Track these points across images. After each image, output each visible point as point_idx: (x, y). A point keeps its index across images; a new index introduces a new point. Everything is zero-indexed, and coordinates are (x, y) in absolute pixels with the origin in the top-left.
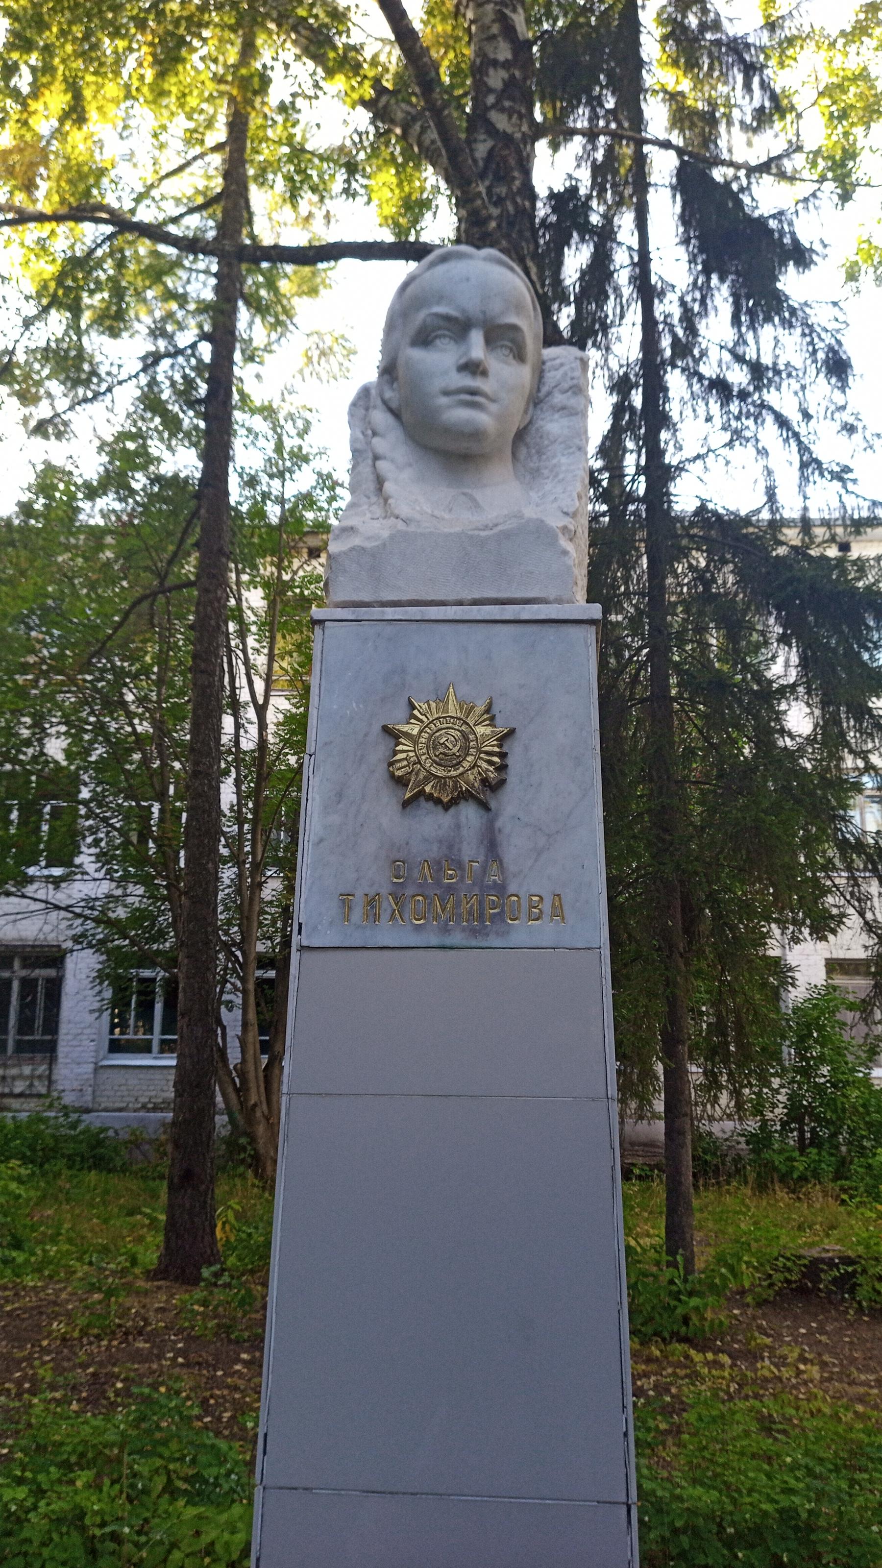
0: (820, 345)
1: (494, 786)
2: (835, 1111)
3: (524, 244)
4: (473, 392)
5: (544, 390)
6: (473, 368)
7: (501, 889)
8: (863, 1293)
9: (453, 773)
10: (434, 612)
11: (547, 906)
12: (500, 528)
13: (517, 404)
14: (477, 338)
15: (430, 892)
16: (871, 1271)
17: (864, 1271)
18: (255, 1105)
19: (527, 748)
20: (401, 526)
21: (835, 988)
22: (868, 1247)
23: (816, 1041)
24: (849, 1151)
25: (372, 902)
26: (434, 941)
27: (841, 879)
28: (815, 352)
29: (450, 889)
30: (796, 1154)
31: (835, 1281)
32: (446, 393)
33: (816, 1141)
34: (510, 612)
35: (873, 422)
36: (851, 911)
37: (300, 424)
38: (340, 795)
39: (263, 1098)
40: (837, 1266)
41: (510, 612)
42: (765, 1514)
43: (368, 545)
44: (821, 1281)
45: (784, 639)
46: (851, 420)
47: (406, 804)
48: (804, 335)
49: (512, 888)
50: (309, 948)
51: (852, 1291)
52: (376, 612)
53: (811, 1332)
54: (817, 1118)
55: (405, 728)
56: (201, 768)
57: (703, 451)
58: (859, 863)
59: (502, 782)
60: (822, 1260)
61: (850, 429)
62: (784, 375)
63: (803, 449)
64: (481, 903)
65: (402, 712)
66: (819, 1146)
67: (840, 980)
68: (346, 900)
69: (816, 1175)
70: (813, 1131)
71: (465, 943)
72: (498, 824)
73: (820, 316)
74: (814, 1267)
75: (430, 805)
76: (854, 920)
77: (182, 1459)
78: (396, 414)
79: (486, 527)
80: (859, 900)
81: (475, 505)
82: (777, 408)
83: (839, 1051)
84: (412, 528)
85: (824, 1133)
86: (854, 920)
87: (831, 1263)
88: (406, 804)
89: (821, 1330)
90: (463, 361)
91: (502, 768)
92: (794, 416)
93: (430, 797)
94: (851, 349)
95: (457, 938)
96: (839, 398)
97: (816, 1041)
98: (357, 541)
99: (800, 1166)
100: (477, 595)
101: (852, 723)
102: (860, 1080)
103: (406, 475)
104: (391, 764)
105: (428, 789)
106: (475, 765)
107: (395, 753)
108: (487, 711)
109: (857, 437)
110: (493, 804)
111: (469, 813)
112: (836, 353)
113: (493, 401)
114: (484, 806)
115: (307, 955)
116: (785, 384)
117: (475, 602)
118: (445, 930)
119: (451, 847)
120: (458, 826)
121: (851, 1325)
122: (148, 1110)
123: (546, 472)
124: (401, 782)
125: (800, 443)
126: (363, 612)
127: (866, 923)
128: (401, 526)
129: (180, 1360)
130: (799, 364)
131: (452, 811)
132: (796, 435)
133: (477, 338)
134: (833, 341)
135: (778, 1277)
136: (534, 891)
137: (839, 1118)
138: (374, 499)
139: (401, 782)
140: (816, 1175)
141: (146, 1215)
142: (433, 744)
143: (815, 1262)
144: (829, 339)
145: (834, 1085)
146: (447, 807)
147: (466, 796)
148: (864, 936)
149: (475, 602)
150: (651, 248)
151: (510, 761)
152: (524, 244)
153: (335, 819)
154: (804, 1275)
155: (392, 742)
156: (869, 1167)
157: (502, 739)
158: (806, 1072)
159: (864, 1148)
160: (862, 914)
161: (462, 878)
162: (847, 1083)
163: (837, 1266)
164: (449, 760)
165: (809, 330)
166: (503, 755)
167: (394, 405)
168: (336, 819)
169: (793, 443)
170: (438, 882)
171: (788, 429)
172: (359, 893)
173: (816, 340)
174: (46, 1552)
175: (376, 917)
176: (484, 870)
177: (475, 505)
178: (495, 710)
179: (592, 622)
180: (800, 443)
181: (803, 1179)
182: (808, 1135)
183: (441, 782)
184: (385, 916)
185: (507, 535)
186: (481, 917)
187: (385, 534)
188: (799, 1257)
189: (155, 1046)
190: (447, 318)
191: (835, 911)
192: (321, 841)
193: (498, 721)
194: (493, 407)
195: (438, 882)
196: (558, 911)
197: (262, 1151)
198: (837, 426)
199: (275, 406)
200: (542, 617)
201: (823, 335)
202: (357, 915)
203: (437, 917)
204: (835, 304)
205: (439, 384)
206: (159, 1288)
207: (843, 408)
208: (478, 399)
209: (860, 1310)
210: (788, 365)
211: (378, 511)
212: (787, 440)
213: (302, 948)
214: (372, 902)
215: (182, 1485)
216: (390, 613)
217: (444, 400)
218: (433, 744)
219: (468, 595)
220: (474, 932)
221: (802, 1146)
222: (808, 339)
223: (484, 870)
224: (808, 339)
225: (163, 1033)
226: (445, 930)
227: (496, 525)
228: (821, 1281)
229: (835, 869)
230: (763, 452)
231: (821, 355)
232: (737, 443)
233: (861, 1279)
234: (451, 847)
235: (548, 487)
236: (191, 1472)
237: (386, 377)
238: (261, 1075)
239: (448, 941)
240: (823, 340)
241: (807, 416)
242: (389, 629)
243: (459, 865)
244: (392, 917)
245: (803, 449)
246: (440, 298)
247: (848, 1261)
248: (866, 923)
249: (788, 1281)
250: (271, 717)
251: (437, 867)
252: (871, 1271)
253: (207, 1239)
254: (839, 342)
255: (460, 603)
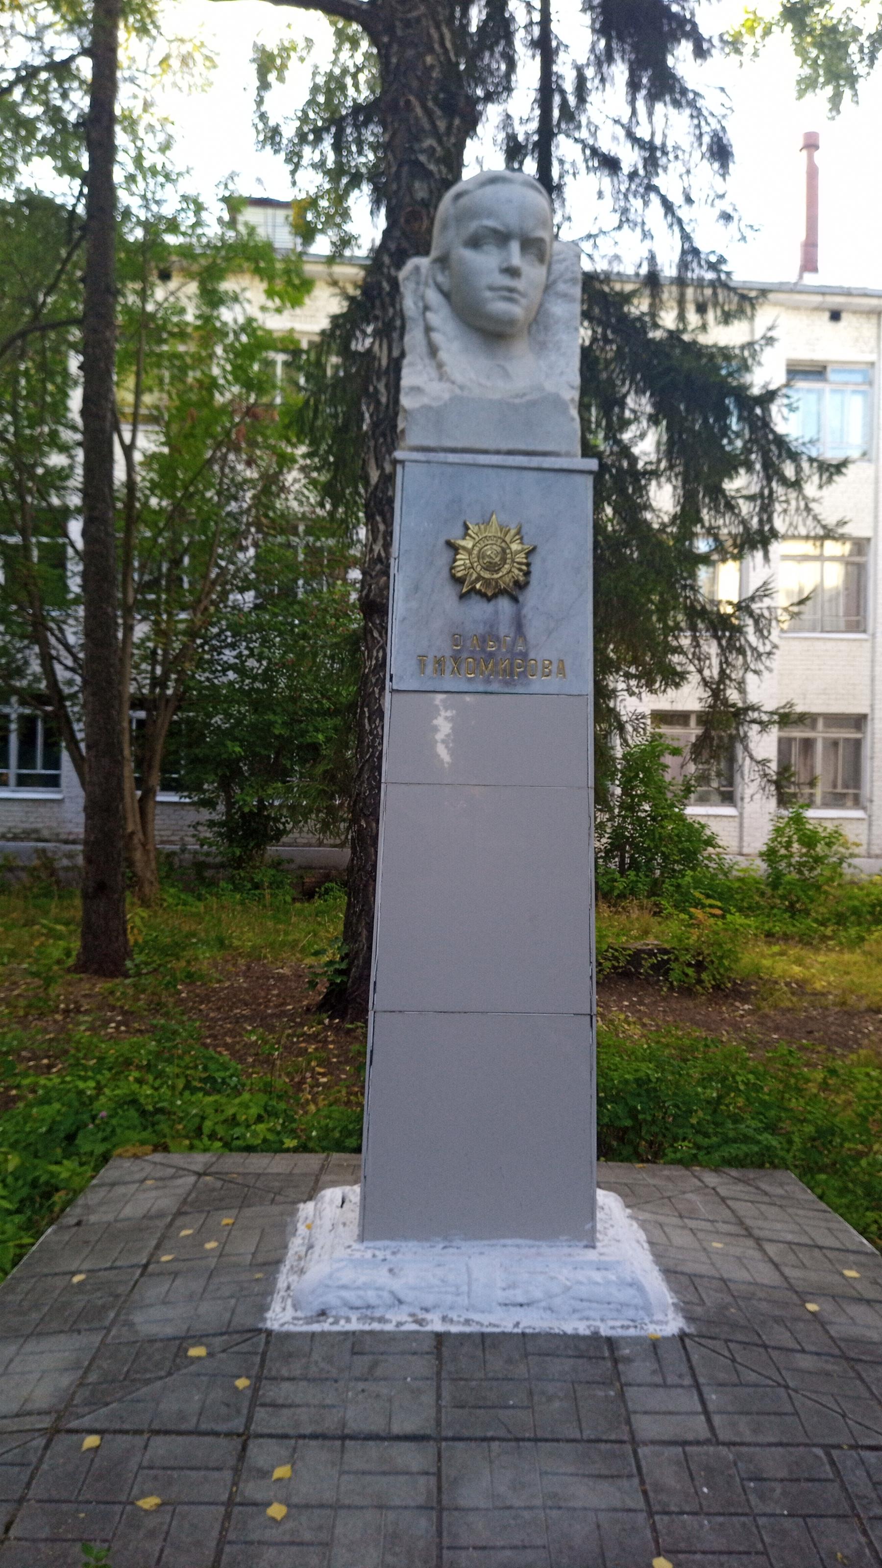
0: (705, 128)
1: (521, 586)
2: (653, 840)
3: (440, 9)
4: (511, 290)
5: (552, 278)
6: (513, 272)
7: (524, 655)
8: (674, 976)
9: (496, 576)
10: (482, 459)
11: (554, 668)
12: (528, 398)
13: (536, 295)
14: (515, 246)
15: (477, 656)
16: (682, 959)
17: (677, 959)
18: (133, 833)
19: (544, 560)
20: (458, 391)
21: (661, 736)
22: (680, 941)
23: (642, 781)
24: (662, 874)
25: (439, 662)
26: (481, 689)
27: (685, 641)
28: (701, 135)
29: (491, 655)
30: (617, 875)
31: (652, 967)
32: (491, 288)
33: (635, 865)
34: (535, 461)
35: (746, 214)
36: (692, 668)
37: (161, 137)
38: (417, 588)
39: (139, 827)
40: (655, 955)
41: (535, 461)
42: (626, 1082)
43: (434, 404)
44: (642, 966)
45: (654, 420)
46: (730, 210)
47: (462, 597)
48: (692, 116)
49: (532, 655)
50: (398, 691)
51: (666, 973)
52: (441, 456)
53: (632, 1004)
54: (635, 846)
55: (462, 543)
56: (96, 514)
57: (594, 232)
58: (701, 625)
59: (527, 583)
60: (643, 951)
61: (727, 217)
62: (671, 156)
63: (686, 237)
64: (511, 664)
65: (459, 530)
66: (637, 869)
67: (665, 730)
68: (422, 661)
69: (633, 892)
70: (632, 857)
71: (501, 690)
72: (525, 611)
73: (710, 103)
74: (636, 957)
75: (478, 598)
76: (694, 678)
77: (196, 1067)
78: (446, 295)
79: (517, 396)
80: (699, 659)
81: (506, 375)
82: (663, 192)
83: (661, 789)
84: (466, 393)
85: (642, 860)
86: (694, 678)
87: (651, 953)
88: (462, 597)
89: (641, 1002)
90: (505, 265)
91: (527, 574)
92: (676, 198)
93: (479, 592)
94: (735, 139)
95: (495, 687)
96: (720, 185)
97: (642, 781)
98: (426, 400)
99: (620, 885)
100: (511, 446)
101: (707, 500)
102: (676, 814)
103: (456, 346)
104: (452, 568)
105: (478, 586)
106: (510, 571)
107: (455, 560)
108: (518, 533)
109: (733, 225)
110: (521, 599)
111: (504, 604)
112: (720, 139)
113: (523, 295)
114: (515, 600)
115: (396, 696)
116: (671, 166)
117: (510, 453)
118: (488, 681)
119: (491, 626)
120: (496, 612)
121: (664, 999)
122: (8, 840)
123: (550, 346)
124: (459, 581)
125: (682, 229)
126: (432, 456)
127: (704, 679)
128: (458, 391)
129: (123, 1028)
130: (686, 146)
131: (493, 603)
132: (680, 222)
133: (515, 246)
134: (718, 127)
135: (608, 964)
136: (546, 656)
137: (656, 847)
138: (427, 361)
139: (459, 581)
140: (633, 892)
141: (44, 926)
142: (481, 556)
143: (638, 952)
144: (715, 125)
145: (654, 819)
146: (489, 599)
147: (501, 592)
148: (701, 689)
149: (510, 453)
150: (552, 10)
151: (533, 569)
152: (440, 9)
153: (414, 604)
154: (628, 962)
155: (451, 553)
156: (678, 886)
157: (530, 553)
158: (630, 808)
159: (674, 870)
160: (700, 671)
161: (499, 648)
162: (665, 817)
163: (655, 955)
164: (492, 567)
165: (697, 114)
166: (528, 565)
167: (446, 288)
168: (414, 604)
169: (676, 228)
170: (483, 650)
171: (673, 214)
172: (431, 656)
173: (703, 123)
174: (114, 1122)
175: (442, 672)
176: (514, 642)
177: (506, 375)
178: (523, 531)
179: (590, 472)
180: (682, 229)
181: (622, 896)
182: (628, 861)
183: (487, 582)
184: (448, 671)
185: (533, 404)
186: (511, 674)
187: (446, 396)
188: (624, 949)
189: (12, 780)
190: (495, 231)
191: (679, 668)
192: (404, 619)
193: (526, 540)
194: (523, 301)
195: (483, 650)
196: (562, 671)
197: (140, 874)
198: (716, 212)
199: (135, 116)
200: (557, 466)
201: (710, 119)
202: (430, 669)
203: (482, 673)
204: (722, 90)
205: (485, 281)
206: (81, 980)
207: (722, 197)
208: (515, 296)
209: (671, 988)
210: (676, 148)
211: (434, 374)
212: (671, 226)
213: (393, 691)
214: (439, 662)
215: (196, 1084)
216: (452, 458)
217: (488, 294)
218: (481, 556)
219: (504, 446)
220: (507, 683)
221: (622, 871)
222: (696, 121)
223: (514, 642)
224: (696, 121)
225: (20, 766)
226: (488, 681)
227: (524, 395)
228: (642, 966)
229: (681, 630)
230: (646, 235)
231: (706, 139)
232: (626, 226)
233: (673, 965)
234: (491, 626)
235: (553, 358)
236: (204, 1075)
237: (438, 265)
238: (136, 805)
239: (490, 688)
240: (708, 124)
241: (689, 200)
242: (450, 470)
243: (497, 639)
244: (453, 672)
245: (686, 237)
246: (490, 214)
247: (665, 951)
248: (704, 679)
249: (614, 967)
250: (138, 457)
251: (483, 640)
252: (682, 959)
253: (121, 938)
254: (723, 128)
255: (498, 452)
